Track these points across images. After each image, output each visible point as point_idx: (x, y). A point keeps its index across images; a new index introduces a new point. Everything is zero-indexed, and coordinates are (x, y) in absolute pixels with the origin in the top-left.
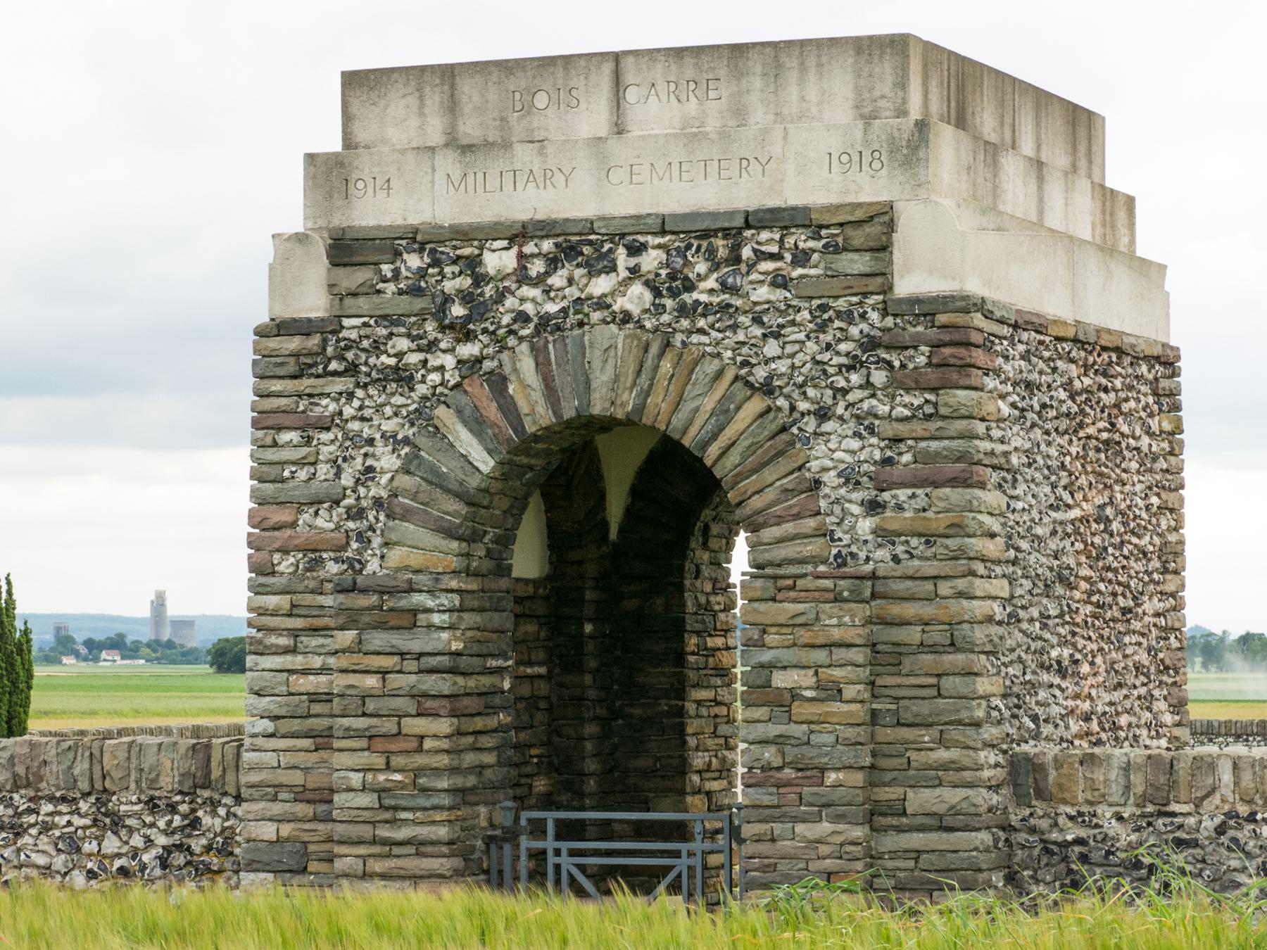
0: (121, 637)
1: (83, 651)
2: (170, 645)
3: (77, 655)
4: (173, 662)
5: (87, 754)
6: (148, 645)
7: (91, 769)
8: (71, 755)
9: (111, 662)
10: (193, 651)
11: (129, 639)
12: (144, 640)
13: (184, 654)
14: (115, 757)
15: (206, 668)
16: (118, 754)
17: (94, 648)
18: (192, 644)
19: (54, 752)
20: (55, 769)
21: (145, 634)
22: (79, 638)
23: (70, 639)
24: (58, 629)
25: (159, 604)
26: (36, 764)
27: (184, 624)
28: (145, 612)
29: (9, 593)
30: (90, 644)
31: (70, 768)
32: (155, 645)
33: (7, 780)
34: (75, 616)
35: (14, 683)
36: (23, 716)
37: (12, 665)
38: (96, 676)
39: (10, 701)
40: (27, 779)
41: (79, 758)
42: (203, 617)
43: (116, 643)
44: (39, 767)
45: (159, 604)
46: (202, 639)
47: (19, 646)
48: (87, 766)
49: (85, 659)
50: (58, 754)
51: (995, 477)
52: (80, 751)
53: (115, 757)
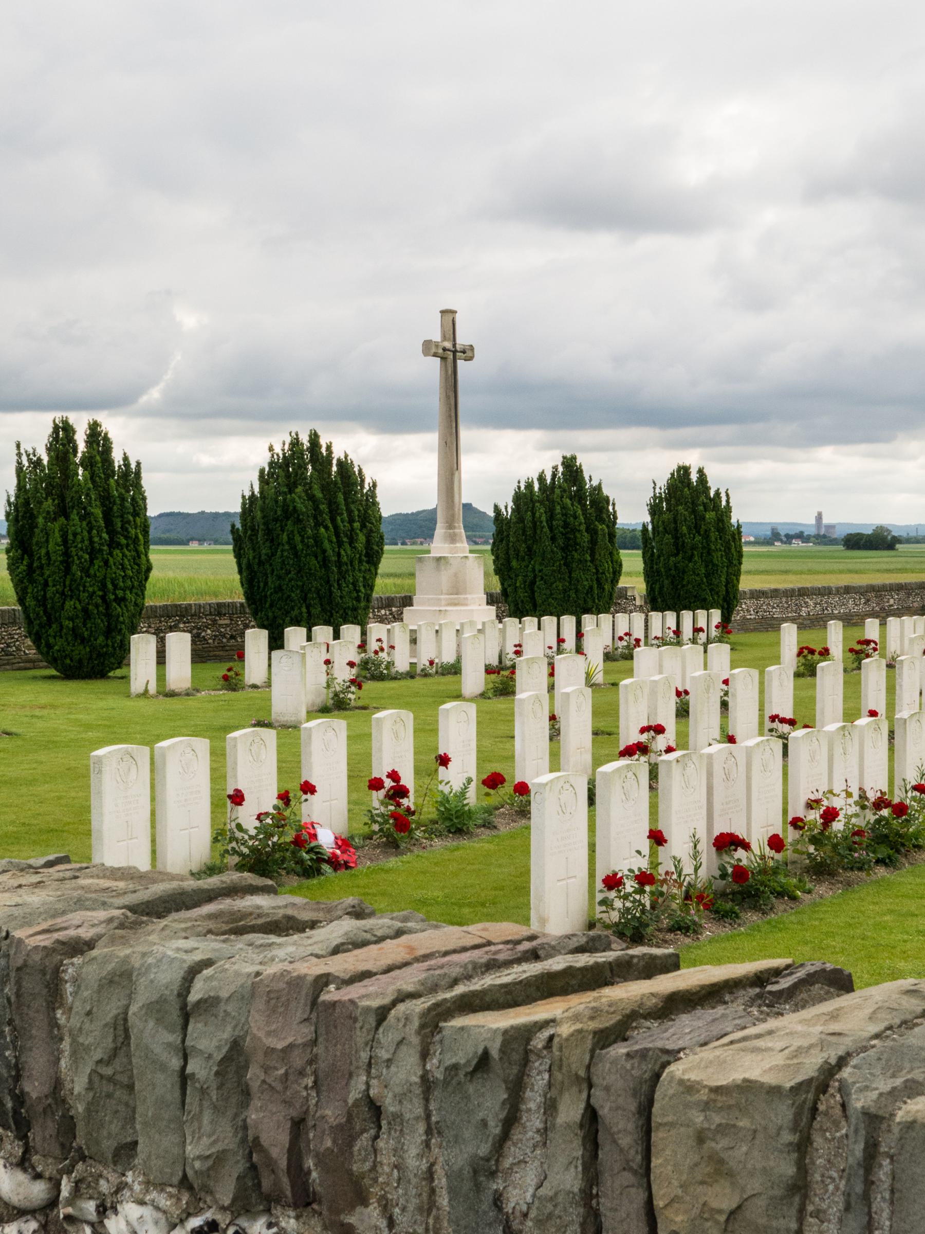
0: (802, 533)
1: (784, 539)
2: (824, 536)
3: (782, 542)
4: (826, 544)
5: (570, 1111)
6: (814, 537)
7: (588, 1196)
8: (490, 1101)
9: (797, 544)
10: (835, 539)
11: (806, 534)
12: (813, 534)
13: (831, 541)
14: (720, 1169)
15: (841, 547)
16: (738, 1153)
17: (789, 538)
18: (835, 536)
19: (407, 1070)
20: (414, 1162)
21: (812, 531)
22: (783, 533)
23: (778, 534)
24: (773, 529)
25: (819, 517)
26: (332, 1113)
27: (831, 527)
28: (813, 522)
29: (728, 502)
30: (787, 536)
31: (486, 1168)
32: (817, 536)
33: (219, 1159)
34: (780, 524)
35: (730, 562)
36: (735, 582)
37: (729, 549)
38: (790, 551)
39: (727, 572)
40: (297, 1171)
41: (533, 1121)
42: (840, 524)
43: (800, 536)
44: (346, 1134)
45: (819, 517)
46: (840, 533)
47: (733, 535)
48: (570, 1179)
49: (785, 543)
50: (427, 1084)
51: (655, 567)
52: (539, 1080)
53: (720, 1169)
